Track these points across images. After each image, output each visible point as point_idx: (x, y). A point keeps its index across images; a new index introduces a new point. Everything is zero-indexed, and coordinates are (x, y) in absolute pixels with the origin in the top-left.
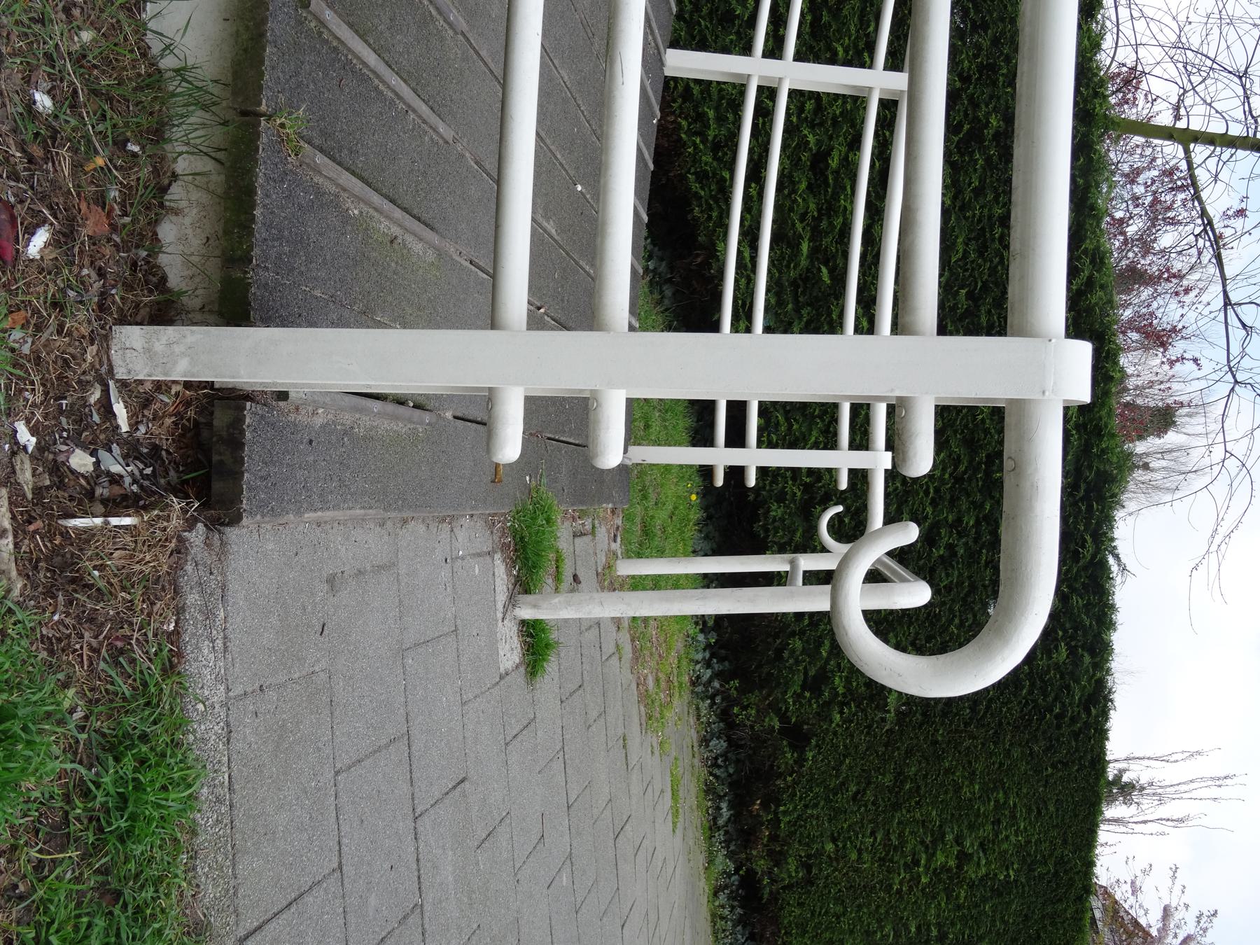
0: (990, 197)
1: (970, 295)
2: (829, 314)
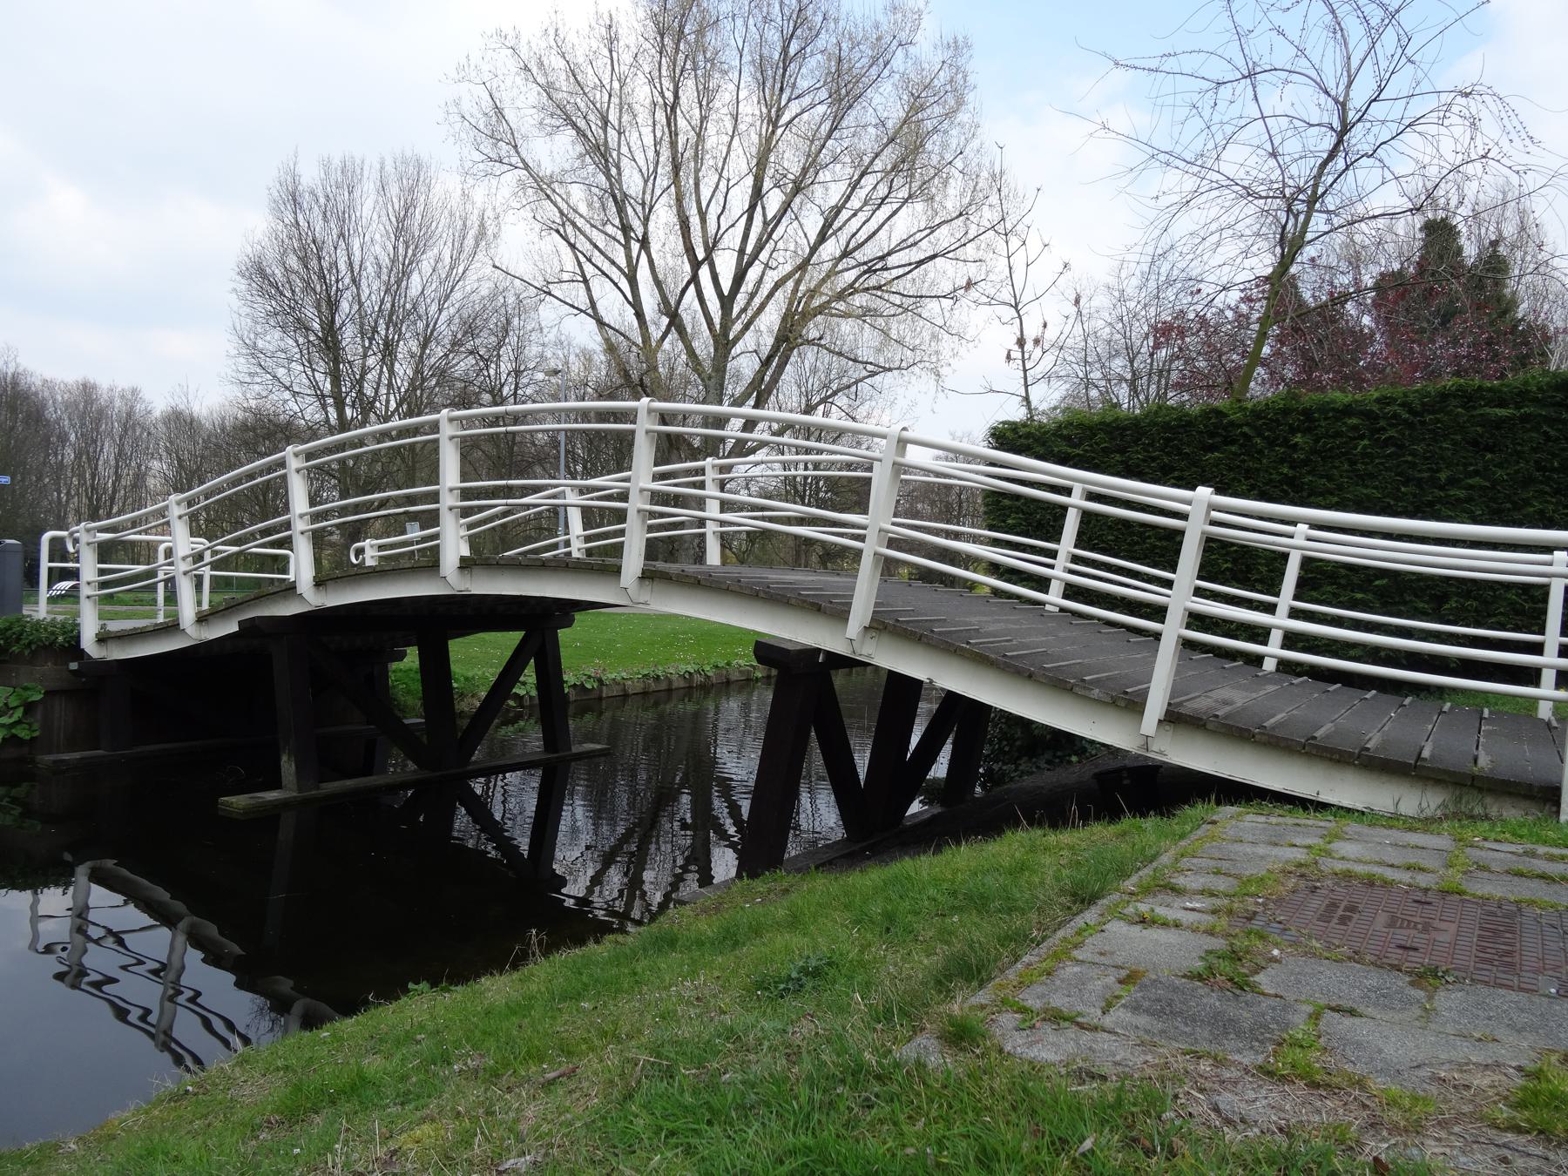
0: (1335, 472)
1: (1405, 484)
2: (1412, 581)
